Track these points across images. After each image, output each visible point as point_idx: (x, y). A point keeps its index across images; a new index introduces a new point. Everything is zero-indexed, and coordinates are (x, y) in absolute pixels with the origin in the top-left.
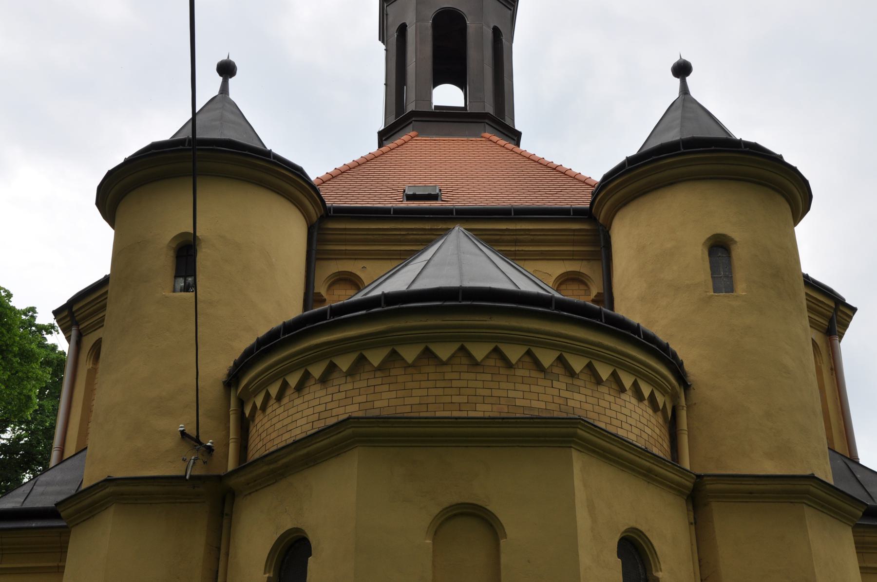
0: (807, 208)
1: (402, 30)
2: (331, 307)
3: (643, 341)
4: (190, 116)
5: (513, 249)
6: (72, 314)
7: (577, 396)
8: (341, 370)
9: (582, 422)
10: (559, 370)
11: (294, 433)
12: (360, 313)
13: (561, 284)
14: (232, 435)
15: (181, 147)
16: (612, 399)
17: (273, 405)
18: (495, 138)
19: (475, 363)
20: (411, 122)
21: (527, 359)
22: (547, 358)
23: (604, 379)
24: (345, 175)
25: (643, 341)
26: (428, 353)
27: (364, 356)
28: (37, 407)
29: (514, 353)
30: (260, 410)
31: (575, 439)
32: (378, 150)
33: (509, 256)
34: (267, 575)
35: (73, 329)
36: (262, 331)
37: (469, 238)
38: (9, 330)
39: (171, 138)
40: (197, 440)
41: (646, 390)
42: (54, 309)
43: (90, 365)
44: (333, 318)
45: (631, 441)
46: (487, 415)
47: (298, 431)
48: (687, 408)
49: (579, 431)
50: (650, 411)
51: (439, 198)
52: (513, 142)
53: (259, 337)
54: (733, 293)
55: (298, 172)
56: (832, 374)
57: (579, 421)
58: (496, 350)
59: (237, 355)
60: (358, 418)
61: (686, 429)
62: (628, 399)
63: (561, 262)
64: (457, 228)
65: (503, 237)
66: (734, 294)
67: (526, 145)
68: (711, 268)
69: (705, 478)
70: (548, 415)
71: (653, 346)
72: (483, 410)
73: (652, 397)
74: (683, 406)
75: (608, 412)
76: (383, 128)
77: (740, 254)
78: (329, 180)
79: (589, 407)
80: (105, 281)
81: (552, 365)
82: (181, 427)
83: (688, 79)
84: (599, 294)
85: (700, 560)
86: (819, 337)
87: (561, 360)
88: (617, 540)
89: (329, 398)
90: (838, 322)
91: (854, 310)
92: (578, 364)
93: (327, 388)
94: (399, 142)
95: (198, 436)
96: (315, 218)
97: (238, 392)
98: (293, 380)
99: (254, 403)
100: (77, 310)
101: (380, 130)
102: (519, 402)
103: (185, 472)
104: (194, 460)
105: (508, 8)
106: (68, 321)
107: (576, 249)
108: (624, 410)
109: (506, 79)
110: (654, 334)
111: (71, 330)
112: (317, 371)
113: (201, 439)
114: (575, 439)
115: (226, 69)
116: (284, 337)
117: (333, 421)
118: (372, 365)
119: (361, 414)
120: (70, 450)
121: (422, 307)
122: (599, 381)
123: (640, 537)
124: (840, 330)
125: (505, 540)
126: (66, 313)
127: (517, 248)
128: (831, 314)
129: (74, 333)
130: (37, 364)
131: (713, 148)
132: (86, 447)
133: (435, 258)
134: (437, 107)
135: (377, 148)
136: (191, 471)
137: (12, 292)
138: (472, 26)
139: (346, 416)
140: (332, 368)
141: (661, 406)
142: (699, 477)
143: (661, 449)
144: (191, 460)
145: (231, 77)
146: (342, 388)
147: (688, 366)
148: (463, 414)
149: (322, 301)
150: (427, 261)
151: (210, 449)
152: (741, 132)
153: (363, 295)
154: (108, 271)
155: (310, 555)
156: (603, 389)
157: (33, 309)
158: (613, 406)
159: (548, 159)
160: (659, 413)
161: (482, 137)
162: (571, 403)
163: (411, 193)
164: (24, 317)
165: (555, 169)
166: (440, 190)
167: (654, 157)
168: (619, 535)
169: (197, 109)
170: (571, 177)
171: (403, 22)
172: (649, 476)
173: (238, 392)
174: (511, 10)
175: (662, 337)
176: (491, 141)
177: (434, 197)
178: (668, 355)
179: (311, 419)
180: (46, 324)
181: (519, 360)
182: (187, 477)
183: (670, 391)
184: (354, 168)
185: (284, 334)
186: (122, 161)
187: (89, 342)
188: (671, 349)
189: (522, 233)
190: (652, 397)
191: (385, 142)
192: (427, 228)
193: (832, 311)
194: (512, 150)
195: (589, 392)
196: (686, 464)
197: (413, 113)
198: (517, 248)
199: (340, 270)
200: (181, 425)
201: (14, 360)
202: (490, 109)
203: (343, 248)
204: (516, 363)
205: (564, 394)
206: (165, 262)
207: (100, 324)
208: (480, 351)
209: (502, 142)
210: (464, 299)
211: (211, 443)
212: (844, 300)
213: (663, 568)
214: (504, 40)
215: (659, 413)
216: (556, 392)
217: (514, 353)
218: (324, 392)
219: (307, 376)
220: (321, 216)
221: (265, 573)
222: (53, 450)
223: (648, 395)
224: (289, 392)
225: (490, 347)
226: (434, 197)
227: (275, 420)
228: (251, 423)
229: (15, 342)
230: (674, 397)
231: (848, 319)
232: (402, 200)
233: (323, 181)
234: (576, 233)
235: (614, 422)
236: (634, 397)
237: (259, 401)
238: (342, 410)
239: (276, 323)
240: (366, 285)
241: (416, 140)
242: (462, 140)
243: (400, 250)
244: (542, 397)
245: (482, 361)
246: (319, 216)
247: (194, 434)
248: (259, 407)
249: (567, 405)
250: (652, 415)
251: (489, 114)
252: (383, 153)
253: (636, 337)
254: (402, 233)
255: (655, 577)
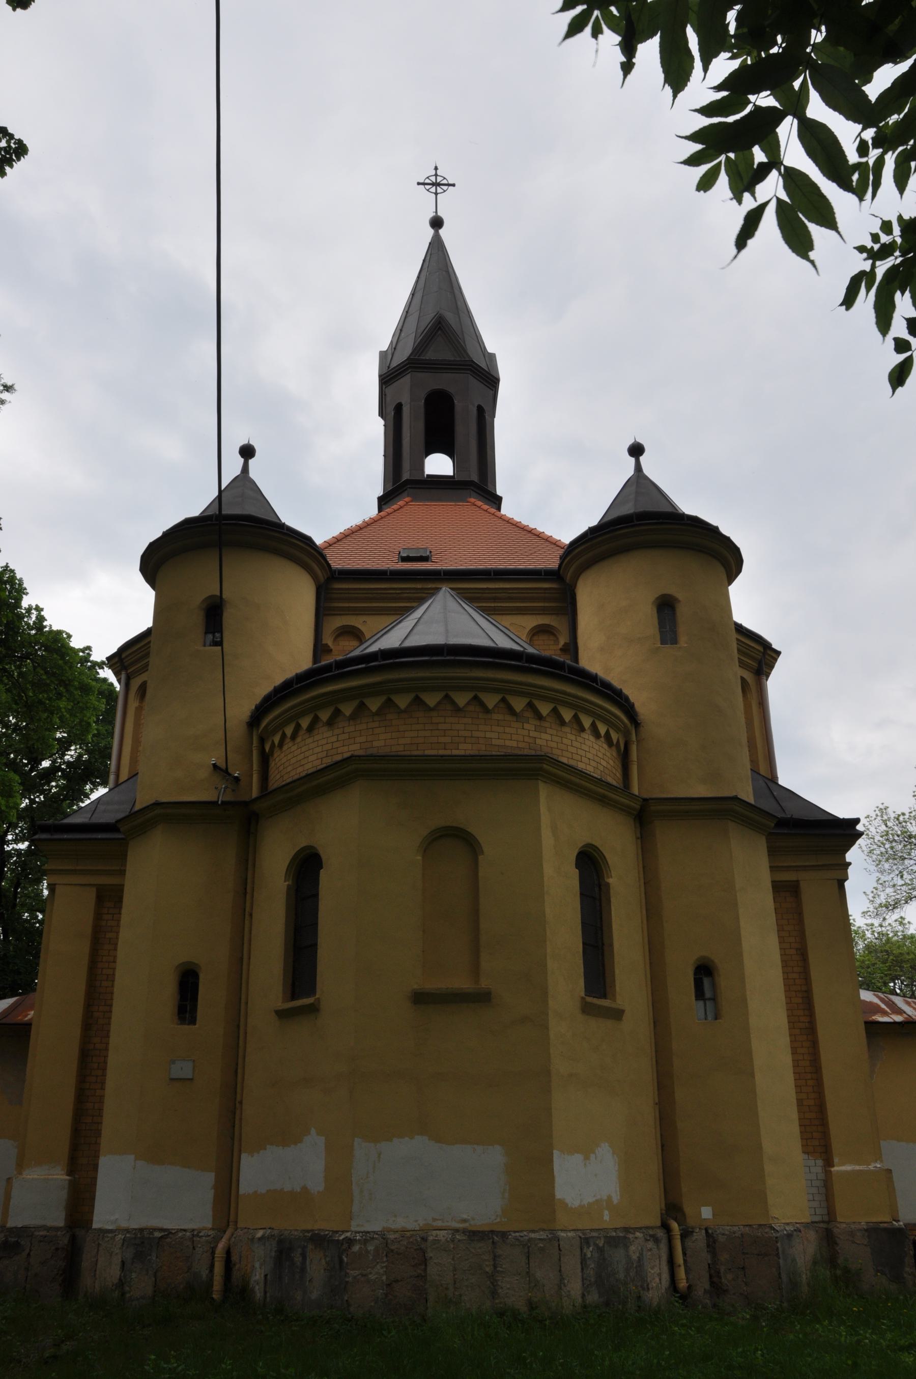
0: (739, 571)
1: (399, 408)
2: (336, 661)
3: (600, 688)
4: (216, 494)
5: (493, 605)
6: (121, 660)
7: (544, 736)
8: (345, 715)
9: (548, 758)
10: (529, 714)
11: (307, 767)
12: (360, 666)
13: (534, 635)
14: (255, 767)
15: (209, 522)
16: (573, 738)
17: (288, 744)
18: (479, 503)
19: (457, 709)
20: (406, 490)
21: (502, 705)
22: (519, 704)
23: (567, 720)
24: (349, 538)
25: (600, 688)
26: (418, 701)
27: (364, 703)
28: (96, 732)
29: (491, 700)
30: (278, 746)
31: (541, 772)
32: (377, 515)
33: (488, 612)
34: (287, 883)
35: (123, 673)
36: (279, 680)
37: (455, 598)
38: (71, 667)
39: (201, 513)
40: (226, 771)
41: (602, 729)
42: (108, 656)
43: (136, 704)
44: (338, 670)
45: (589, 773)
46: (468, 753)
47: (310, 765)
48: (637, 742)
49: (545, 766)
50: (605, 746)
51: (430, 560)
52: (494, 506)
53: (276, 685)
54: (676, 644)
55: (308, 540)
56: (760, 708)
57: (544, 757)
58: (476, 698)
59: (258, 700)
60: (359, 756)
61: (636, 760)
62: (587, 737)
63: (534, 616)
64: (444, 589)
65: (485, 595)
66: (678, 646)
67: (507, 510)
68: (659, 623)
69: (650, 801)
70: (520, 753)
71: (609, 692)
72: (465, 749)
73: (607, 734)
74: (634, 741)
75: (570, 749)
76: (382, 494)
77: (683, 612)
78: (335, 543)
79: (554, 745)
80: (148, 633)
81: (523, 710)
82: (213, 761)
83: (641, 458)
84: (566, 644)
85: (644, 867)
86: (748, 676)
87: (530, 705)
88: (575, 854)
89: (335, 739)
90: (766, 664)
91: (778, 653)
92: (545, 709)
93: (333, 730)
94: (395, 507)
95: (227, 768)
96: (322, 580)
97: (260, 731)
98: (305, 723)
99: (273, 741)
100: (127, 657)
101: (380, 495)
102: (495, 742)
103: (217, 798)
104: (224, 788)
105: (490, 389)
106: (118, 667)
107: (547, 605)
108: (584, 747)
109: (488, 450)
110: (609, 682)
111: (121, 674)
112: (324, 716)
113: (230, 770)
114: (541, 772)
115: (247, 452)
116: (297, 686)
117: (339, 758)
118: (371, 711)
119: (361, 753)
120: (124, 776)
121: (413, 662)
122: (562, 723)
123: (595, 850)
124: (767, 671)
125: (482, 856)
126: (116, 660)
127: (496, 605)
128: (760, 657)
129: (123, 676)
130: (94, 696)
131: (661, 521)
132: (137, 772)
133: (425, 617)
134: (428, 476)
135: (377, 512)
136: (222, 797)
137: (71, 634)
138: (458, 404)
139: (348, 755)
140: (337, 713)
141: (615, 742)
142: (645, 800)
143: (615, 778)
144: (222, 788)
145: (251, 458)
146: (346, 730)
147: (638, 706)
148: (448, 752)
149: (329, 651)
150: (417, 620)
151: (237, 779)
152: (687, 507)
153: (362, 651)
154: (150, 624)
155: (322, 868)
156: (567, 729)
157: (89, 648)
158: (575, 744)
159: (525, 523)
160: (614, 748)
161: (468, 502)
162: (538, 741)
163: (406, 555)
164: (81, 654)
165: (530, 532)
166: (431, 552)
167: (612, 528)
168: (578, 849)
169: (223, 488)
170: (544, 539)
171: (399, 401)
172: (603, 801)
173: (260, 731)
174: (493, 390)
175: (616, 683)
176: (475, 505)
177: (425, 559)
178: (620, 698)
179: (320, 755)
180: (99, 661)
181: (495, 706)
182: (220, 802)
183: (622, 729)
184: (356, 532)
185: (297, 684)
186: (159, 534)
187: (136, 683)
188: (624, 694)
189: (501, 591)
190: (607, 734)
191: (384, 507)
192: (418, 587)
193: (761, 654)
194: (493, 514)
195: (554, 732)
196: (635, 790)
197: (408, 482)
198: (496, 605)
199: (345, 624)
200: (213, 759)
201: (76, 692)
202: (475, 477)
203: (347, 605)
204: (493, 708)
205: (532, 734)
206: (197, 620)
207: (145, 668)
208: (461, 699)
209: (486, 507)
210: (448, 655)
211: (238, 774)
212: (771, 645)
213: (613, 875)
214: (487, 417)
215: (614, 748)
216: (525, 733)
217: (491, 700)
218: (330, 734)
219: (316, 719)
220: (327, 578)
221: (285, 881)
222: (110, 774)
223: (604, 732)
224: (301, 733)
225: (470, 695)
226: (425, 559)
227: (290, 756)
228: (270, 757)
229: (75, 677)
230: (626, 734)
231: (773, 661)
232: (397, 561)
233: (329, 544)
234: (546, 592)
235: (575, 756)
236: (593, 736)
237: (277, 740)
238: (346, 749)
239: (289, 674)
240: (367, 639)
241: (411, 505)
242: (451, 505)
243: (395, 607)
244: (514, 737)
245: (464, 707)
246: (326, 578)
247: (223, 766)
248: (276, 744)
249: (535, 743)
250: (607, 749)
251: (475, 482)
252: (382, 518)
253: (594, 685)
254: (398, 592)
255: (607, 882)
